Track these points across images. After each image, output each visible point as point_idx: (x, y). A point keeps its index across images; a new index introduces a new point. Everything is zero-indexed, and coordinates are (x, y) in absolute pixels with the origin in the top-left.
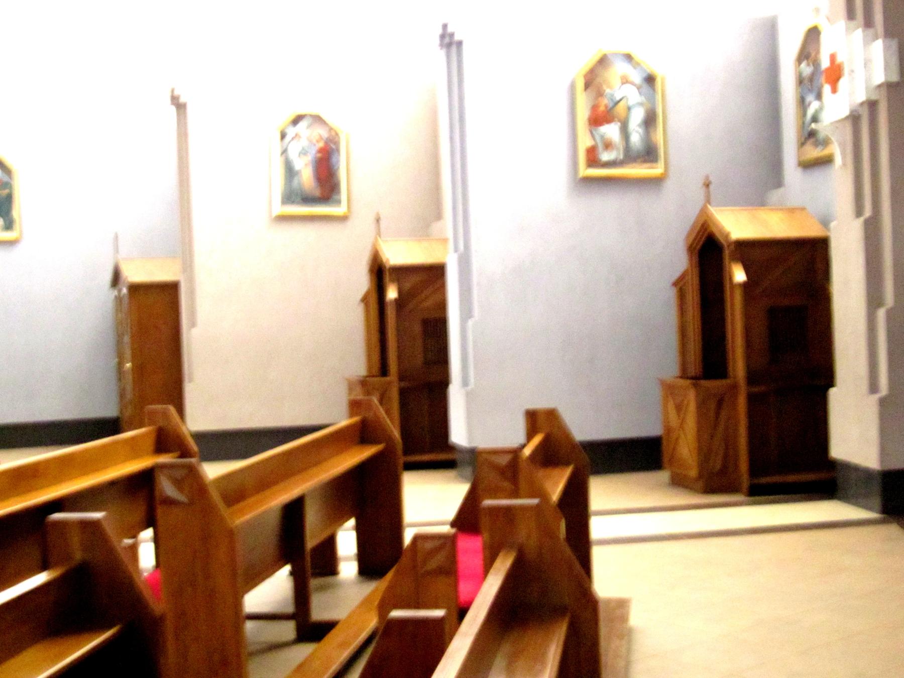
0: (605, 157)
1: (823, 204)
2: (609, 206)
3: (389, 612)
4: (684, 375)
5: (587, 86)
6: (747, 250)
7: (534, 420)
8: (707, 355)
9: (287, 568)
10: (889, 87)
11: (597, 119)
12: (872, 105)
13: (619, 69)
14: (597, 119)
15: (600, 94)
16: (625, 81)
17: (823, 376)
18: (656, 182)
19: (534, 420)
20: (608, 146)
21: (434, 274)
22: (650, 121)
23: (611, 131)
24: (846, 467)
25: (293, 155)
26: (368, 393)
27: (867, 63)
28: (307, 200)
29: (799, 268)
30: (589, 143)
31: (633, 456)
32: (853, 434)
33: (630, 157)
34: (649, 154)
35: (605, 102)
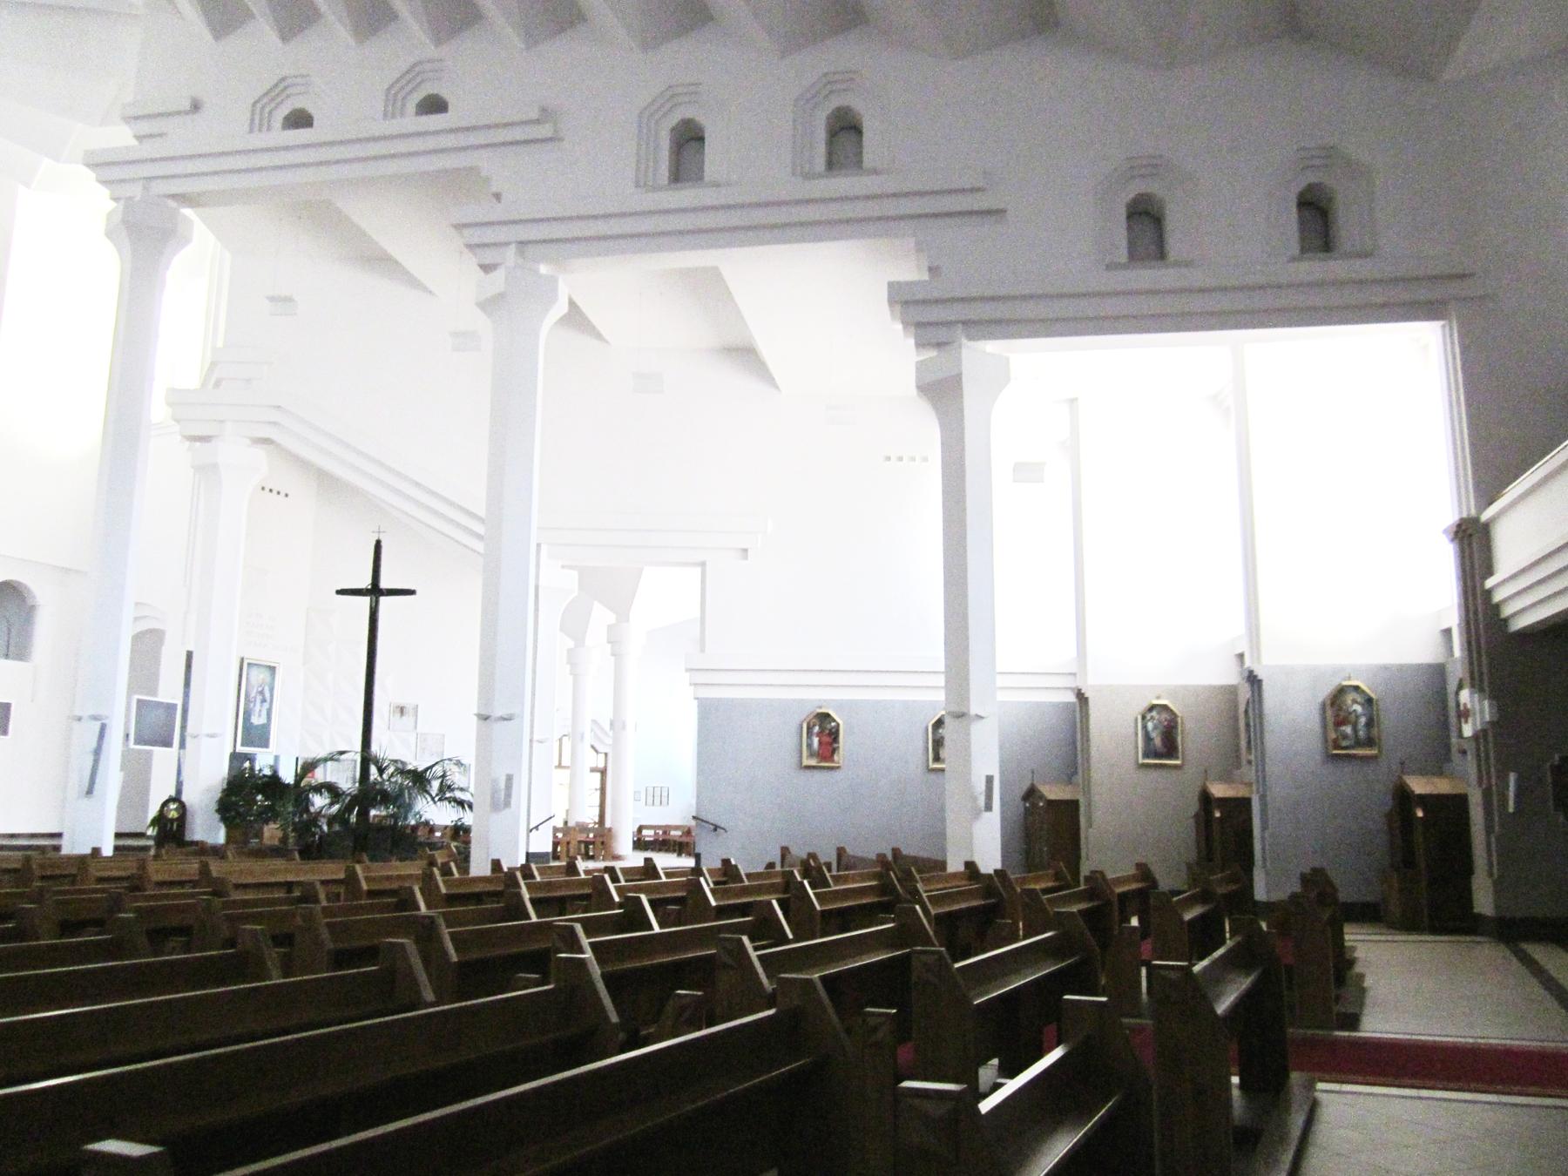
0: (1344, 743)
1: (1462, 779)
2: (1347, 775)
3: (1213, 1011)
4: (1392, 866)
5: (1332, 704)
6: (1424, 800)
7: (1139, 866)
8: (1404, 859)
9: (995, 1061)
10: (1492, 723)
11: (1339, 723)
12: (1484, 731)
13: (1349, 698)
14: (1339, 723)
15: (1340, 709)
16: (1354, 701)
17: (1468, 870)
18: (1374, 758)
19: (1139, 866)
20: (1345, 737)
21: (1243, 804)
22: (1370, 724)
23: (1348, 729)
24: (1480, 915)
25: (1150, 725)
26: (1087, 879)
27: (1482, 711)
28: (1157, 755)
29: (1451, 809)
30: (1333, 736)
31: (1369, 914)
32: (1484, 901)
33: (1358, 744)
34: (1370, 742)
35: (1342, 714)
